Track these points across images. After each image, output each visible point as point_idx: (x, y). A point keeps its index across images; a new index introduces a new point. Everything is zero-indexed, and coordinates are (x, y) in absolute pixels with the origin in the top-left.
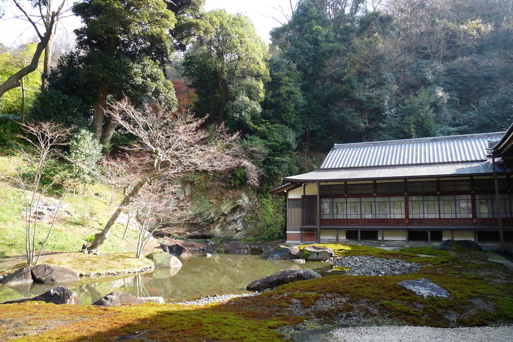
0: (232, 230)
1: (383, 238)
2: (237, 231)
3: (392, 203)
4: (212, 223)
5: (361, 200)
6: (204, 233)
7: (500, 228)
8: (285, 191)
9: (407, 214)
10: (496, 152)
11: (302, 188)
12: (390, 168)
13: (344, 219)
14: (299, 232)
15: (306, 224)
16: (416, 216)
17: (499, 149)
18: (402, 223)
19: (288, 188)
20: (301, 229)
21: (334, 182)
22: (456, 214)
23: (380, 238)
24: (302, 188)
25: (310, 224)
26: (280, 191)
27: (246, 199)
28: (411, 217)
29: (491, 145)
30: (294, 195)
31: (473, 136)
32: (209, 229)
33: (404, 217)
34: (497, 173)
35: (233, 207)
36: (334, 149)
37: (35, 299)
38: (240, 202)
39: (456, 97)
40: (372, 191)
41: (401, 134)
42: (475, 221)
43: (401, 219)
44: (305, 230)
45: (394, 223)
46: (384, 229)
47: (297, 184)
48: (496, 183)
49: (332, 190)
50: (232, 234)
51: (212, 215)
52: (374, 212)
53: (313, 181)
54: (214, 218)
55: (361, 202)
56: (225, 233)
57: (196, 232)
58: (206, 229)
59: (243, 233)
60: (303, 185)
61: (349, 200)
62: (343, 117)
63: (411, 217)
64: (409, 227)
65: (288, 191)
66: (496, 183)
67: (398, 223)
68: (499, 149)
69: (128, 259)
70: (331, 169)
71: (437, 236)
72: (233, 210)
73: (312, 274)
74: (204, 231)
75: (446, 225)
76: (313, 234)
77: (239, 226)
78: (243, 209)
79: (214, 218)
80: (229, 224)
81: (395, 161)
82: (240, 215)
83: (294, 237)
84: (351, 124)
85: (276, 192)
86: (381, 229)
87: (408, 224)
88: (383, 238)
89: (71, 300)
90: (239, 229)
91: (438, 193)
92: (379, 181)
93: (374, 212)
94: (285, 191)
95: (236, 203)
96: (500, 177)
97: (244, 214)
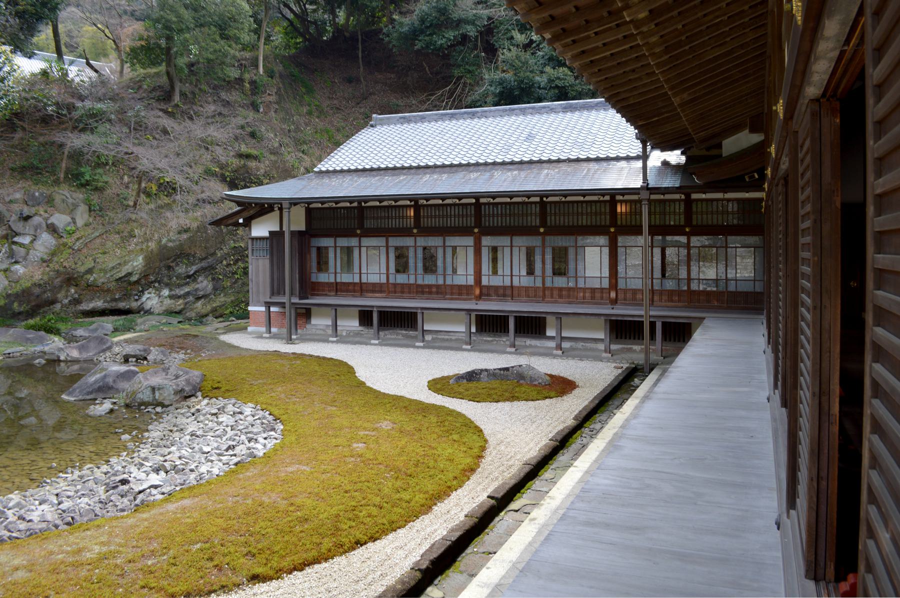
55: (387, 247)
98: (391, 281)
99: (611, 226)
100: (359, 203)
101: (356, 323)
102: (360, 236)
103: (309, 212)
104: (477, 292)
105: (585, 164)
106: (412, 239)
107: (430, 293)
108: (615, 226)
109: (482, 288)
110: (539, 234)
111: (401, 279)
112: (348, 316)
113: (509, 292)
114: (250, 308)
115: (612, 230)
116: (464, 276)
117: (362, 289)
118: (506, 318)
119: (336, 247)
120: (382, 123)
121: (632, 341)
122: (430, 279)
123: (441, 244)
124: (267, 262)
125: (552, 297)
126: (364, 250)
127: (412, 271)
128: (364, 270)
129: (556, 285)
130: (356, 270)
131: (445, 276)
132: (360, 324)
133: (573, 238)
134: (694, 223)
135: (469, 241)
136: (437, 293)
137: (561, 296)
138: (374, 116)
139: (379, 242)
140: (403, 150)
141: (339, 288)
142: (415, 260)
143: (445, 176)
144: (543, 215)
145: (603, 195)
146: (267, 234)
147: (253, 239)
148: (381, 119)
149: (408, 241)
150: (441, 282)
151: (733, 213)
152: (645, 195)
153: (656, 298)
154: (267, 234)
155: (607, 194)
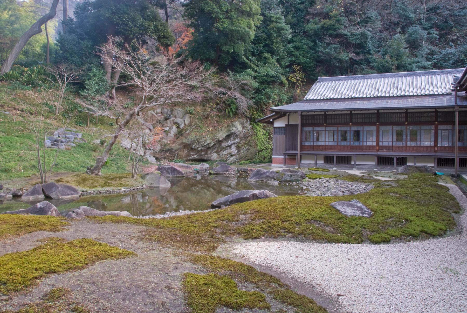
0: (227, 155)
1: (355, 162)
2: (232, 156)
3: (422, 131)
4: (209, 148)
5: (314, 129)
6: (202, 157)
7: (456, 156)
8: (271, 120)
9: (436, 141)
10: (460, 86)
11: (286, 117)
12: (319, 102)
13: (322, 146)
14: (283, 157)
15: (289, 150)
16: (386, 144)
17: (461, 83)
18: (373, 149)
19: (274, 117)
20: (285, 155)
21: (314, 112)
22: (325, 142)
23: (353, 163)
24: (286, 117)
25: (292, 150)
26: (266, 120)
27: (240, 128)
28: (381, 144)
29: (455, 80)
30: (280, 124)
31: (442, 72)
32: (206, 153)
33: (433, 144)
34: (458, 106)
35: (227, 134)
36: (318, 82)
37: (23, 212)
38: (233, 130)
39: (436, 34)
40: (404, 119)
41: (384, 70)
42: (436, 149)
43: (373, 146)
44: (289, 155)
45: (366, 149)
46: (356, 155)
47: (281, 114)
48: (457, 114)
49: (313, 119)
50: (227, 158)
51: (208, 142)
52: (335, 140)
53: (296, 112)
54: (210, 143)
55: (393, 130)
56: (220, 157)
57: (195, 156)
58: (203, 153)
59: (237, 156)
60: (287, 114)
61: (328, 128)
62: (328, 53)
63: (381, 144)
64: (380, 153)
65: (274, 120)
66: (457, 114)
67: (370, 149)
68: (461, 83)
69: (124, 179)
70: (314, 101)
71: (402, 161)
72: (228, 137)
73: (268, 195)
74: (201, 155)
75: (411, 152)
76: (295, 159)
77: (234, 150)
78: (237, 136)
79: (210, 143)
80: (224, 149)
81: (389, 93)
82: (234, 142)
83: (278, 162)
84: (335, 58)
85: (263, 121)
86: (354, 155)
87: (378, 151)
88: (355, 162)
89: (52, 212)
90: (233, 153)
91: (406, 123)
92: (383, 111)
93: (335, 140)
94: (271, 120)
95: (230, 131)
96: (460, 109)
97: (237, 140)
98: (339, 144)
99: (435, 121)
100: (325, 113)
101: (322, 162)
102: (326, 126)
103: (302, 116)
104: (378, 148)
105: (441, 97)
106: (349, 127)
107: (356, 149)
108: (437, 121)
109: (379, 147)
110: (434, 124)
111: (344, 143)
112: (320, 160)
113: (324, 148)
114: (273, 157)
115: (436, 123)
116: (370, 142)
117: (325, 148)
118: (333, 157)
119: (325, 131)
120: (323, 81)
121: (447, 167)
122: (357, 144)
123: (391, 129)
124: (284, 137)
125: (410, 150)
126: (327, 132)
127: (348, 140)
128: (327, 140)
129: (342, 144)
130: (312, 140)
131: (313, 142)
132: (324, 162)
133: (419, 126)
134: (409, 121)
135: (374, 128)
136: (360, 149)
137: (413, 150)
138: (319, 77)
139: (390, 128)
140: (329, 92)
141: (313, 148)
142: (350, 136)
143: (366, 102)
144: (406, 117)
145: (321, 112)
146: (284, 126)
147: (275, 128)
148: (322, 79)
149: (347, 128)
150: (361, 145)
151: (403, 117)
152: (457, 108)
153: (408, 148)
154: (284, 126)
155: (376, 110)
